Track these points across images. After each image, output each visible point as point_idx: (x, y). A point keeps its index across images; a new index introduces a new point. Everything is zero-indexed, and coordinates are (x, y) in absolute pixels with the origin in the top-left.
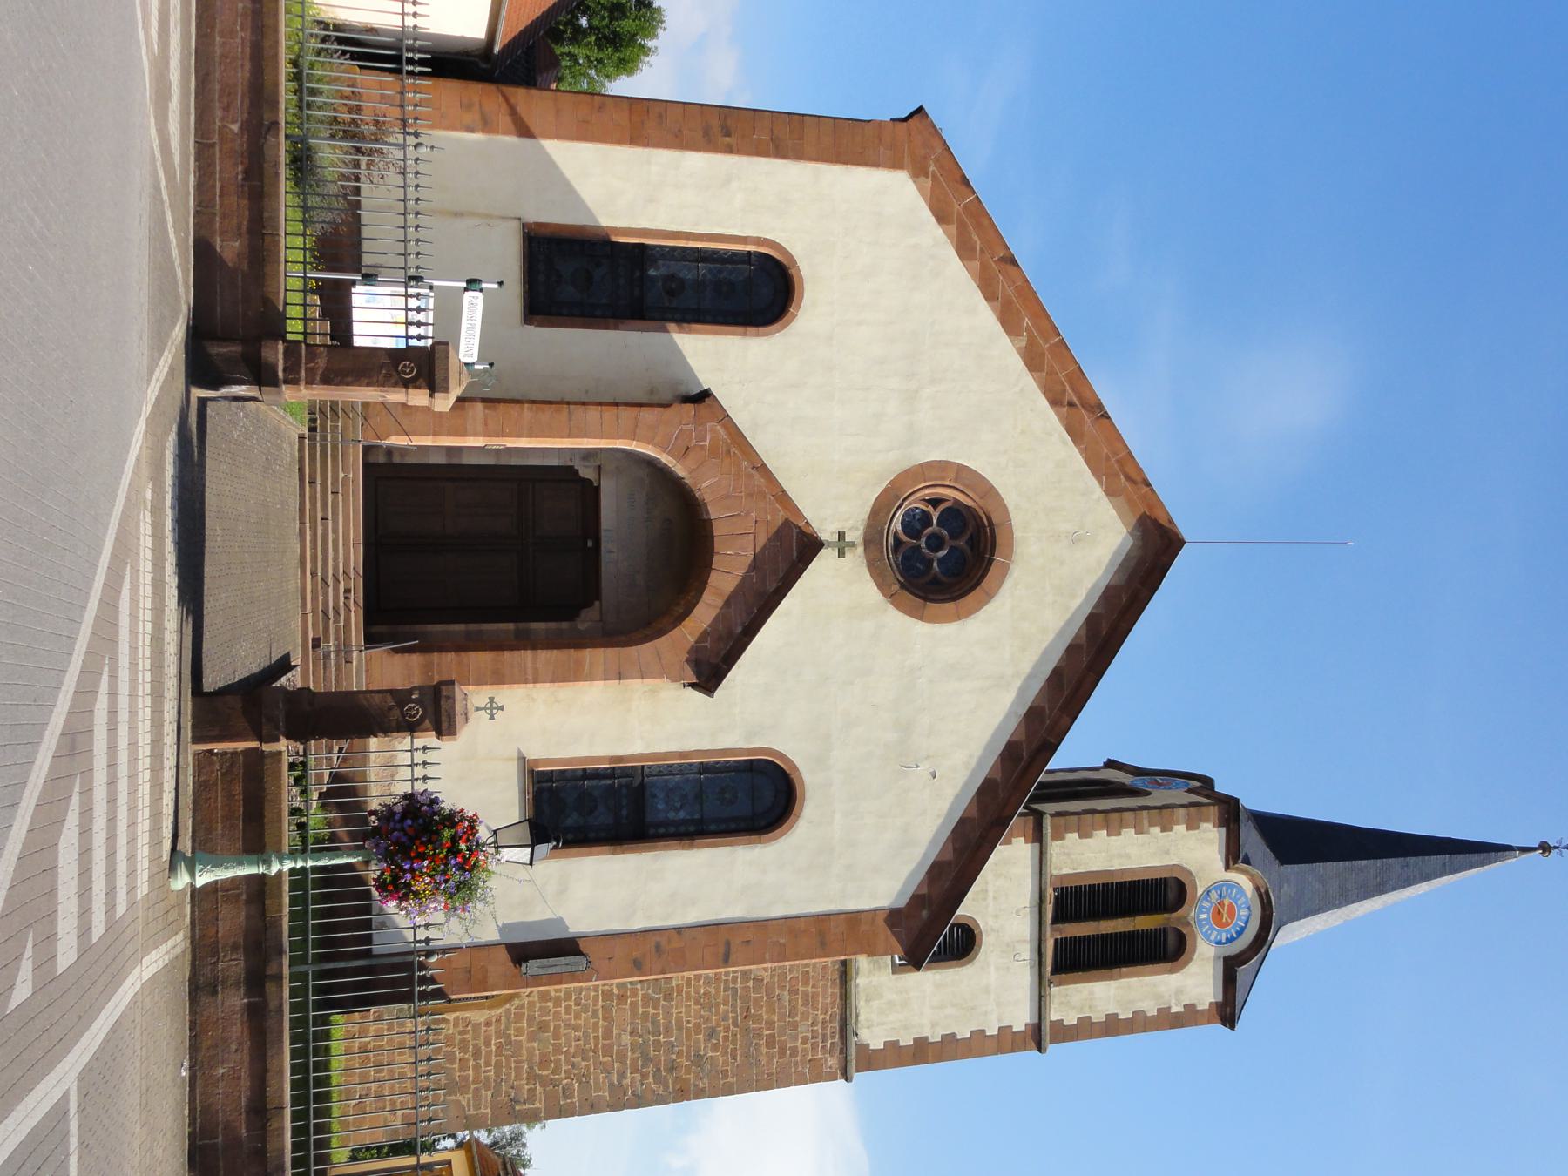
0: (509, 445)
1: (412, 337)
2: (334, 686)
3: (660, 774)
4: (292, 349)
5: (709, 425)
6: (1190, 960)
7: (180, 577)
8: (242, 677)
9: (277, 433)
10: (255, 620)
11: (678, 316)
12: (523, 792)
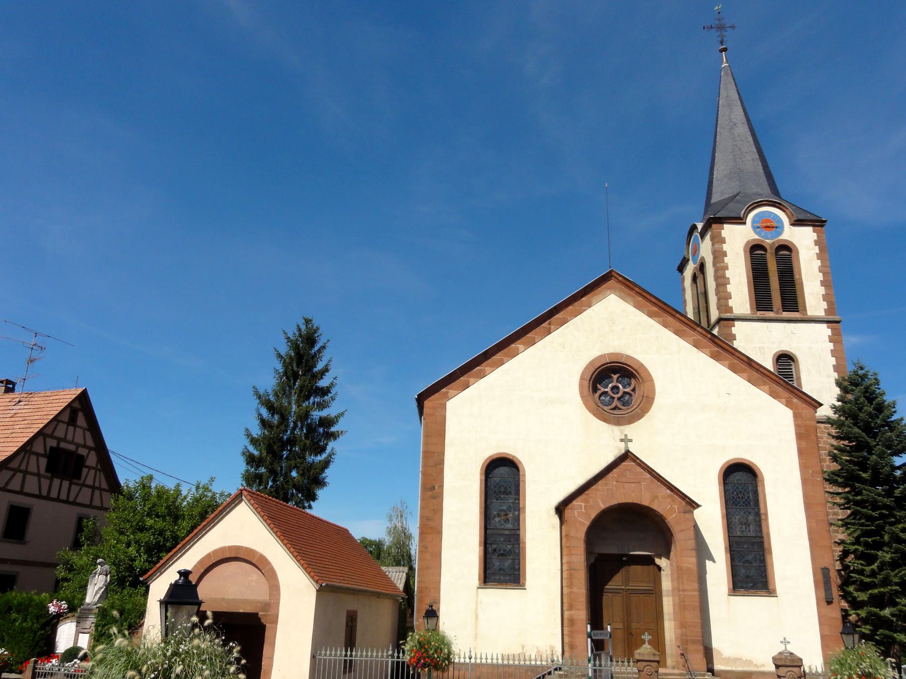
6: (791, 243)
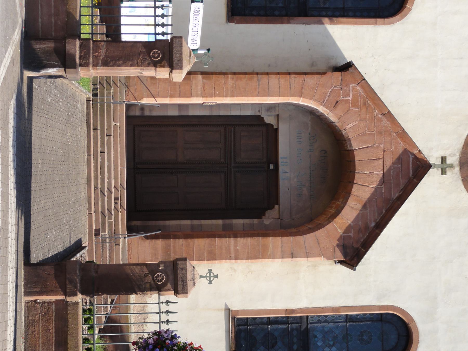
0: (218, 102)
1: (159, 34)
2: (108, 260)
3: (319, 322)
4: (84, 44)
5: (351, 86)
7: (17, 190)
8: (53, 254)
9: (74, 97)
10: (61, 217)
11: (330, 13)
12: (229, 332)
